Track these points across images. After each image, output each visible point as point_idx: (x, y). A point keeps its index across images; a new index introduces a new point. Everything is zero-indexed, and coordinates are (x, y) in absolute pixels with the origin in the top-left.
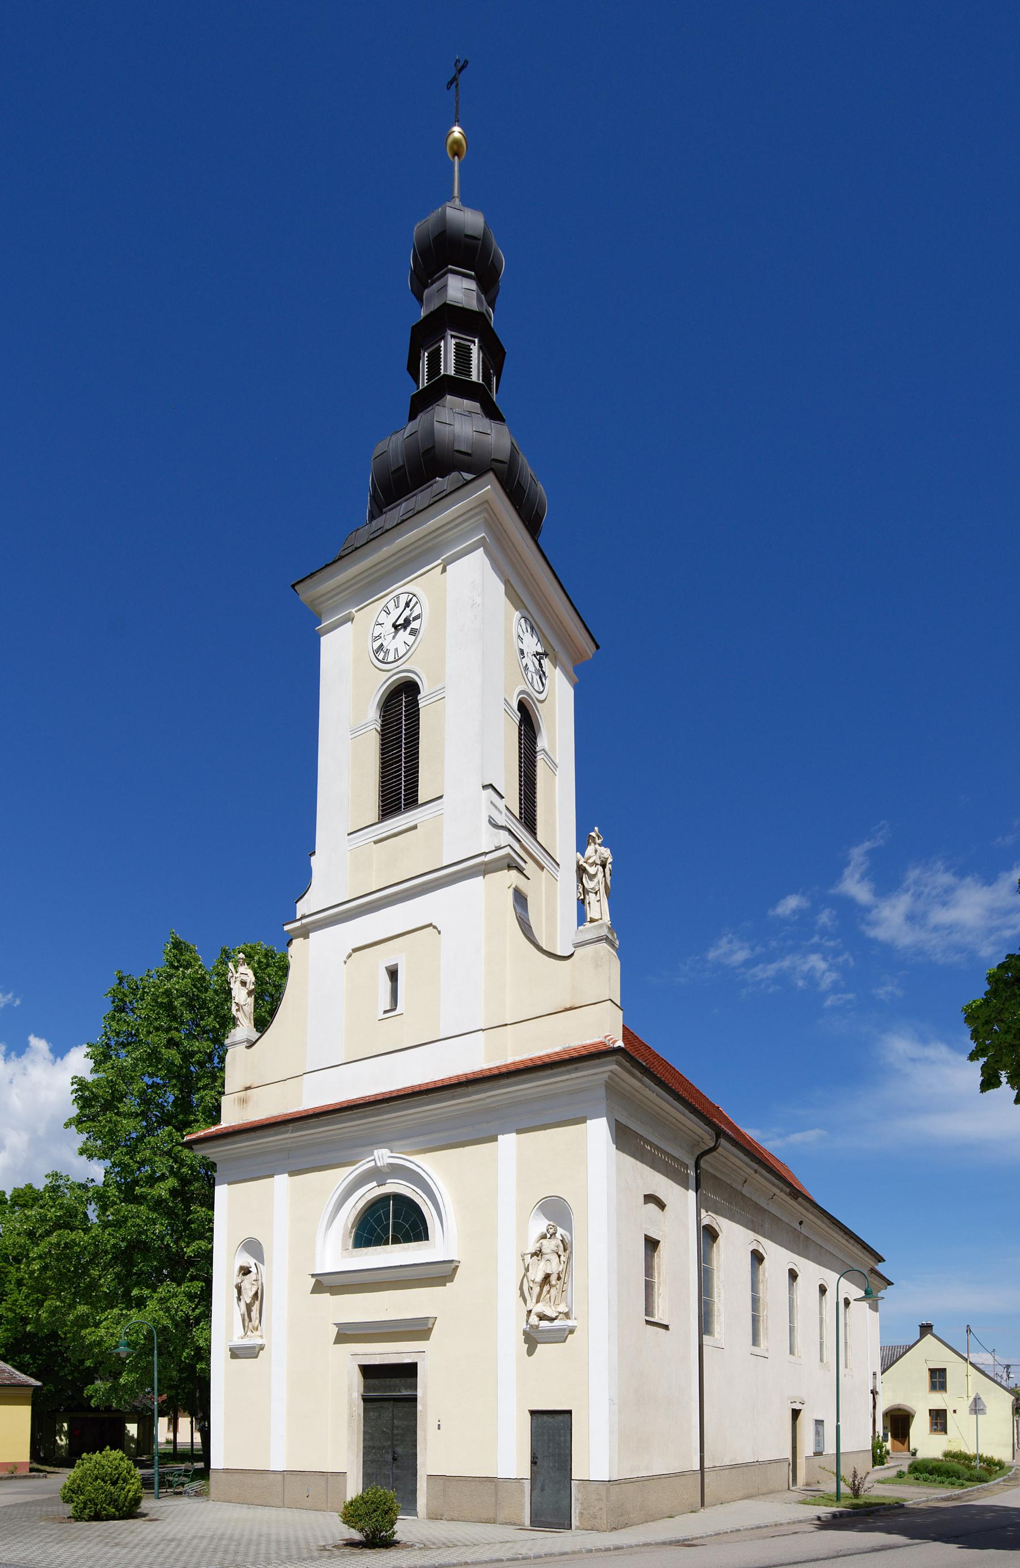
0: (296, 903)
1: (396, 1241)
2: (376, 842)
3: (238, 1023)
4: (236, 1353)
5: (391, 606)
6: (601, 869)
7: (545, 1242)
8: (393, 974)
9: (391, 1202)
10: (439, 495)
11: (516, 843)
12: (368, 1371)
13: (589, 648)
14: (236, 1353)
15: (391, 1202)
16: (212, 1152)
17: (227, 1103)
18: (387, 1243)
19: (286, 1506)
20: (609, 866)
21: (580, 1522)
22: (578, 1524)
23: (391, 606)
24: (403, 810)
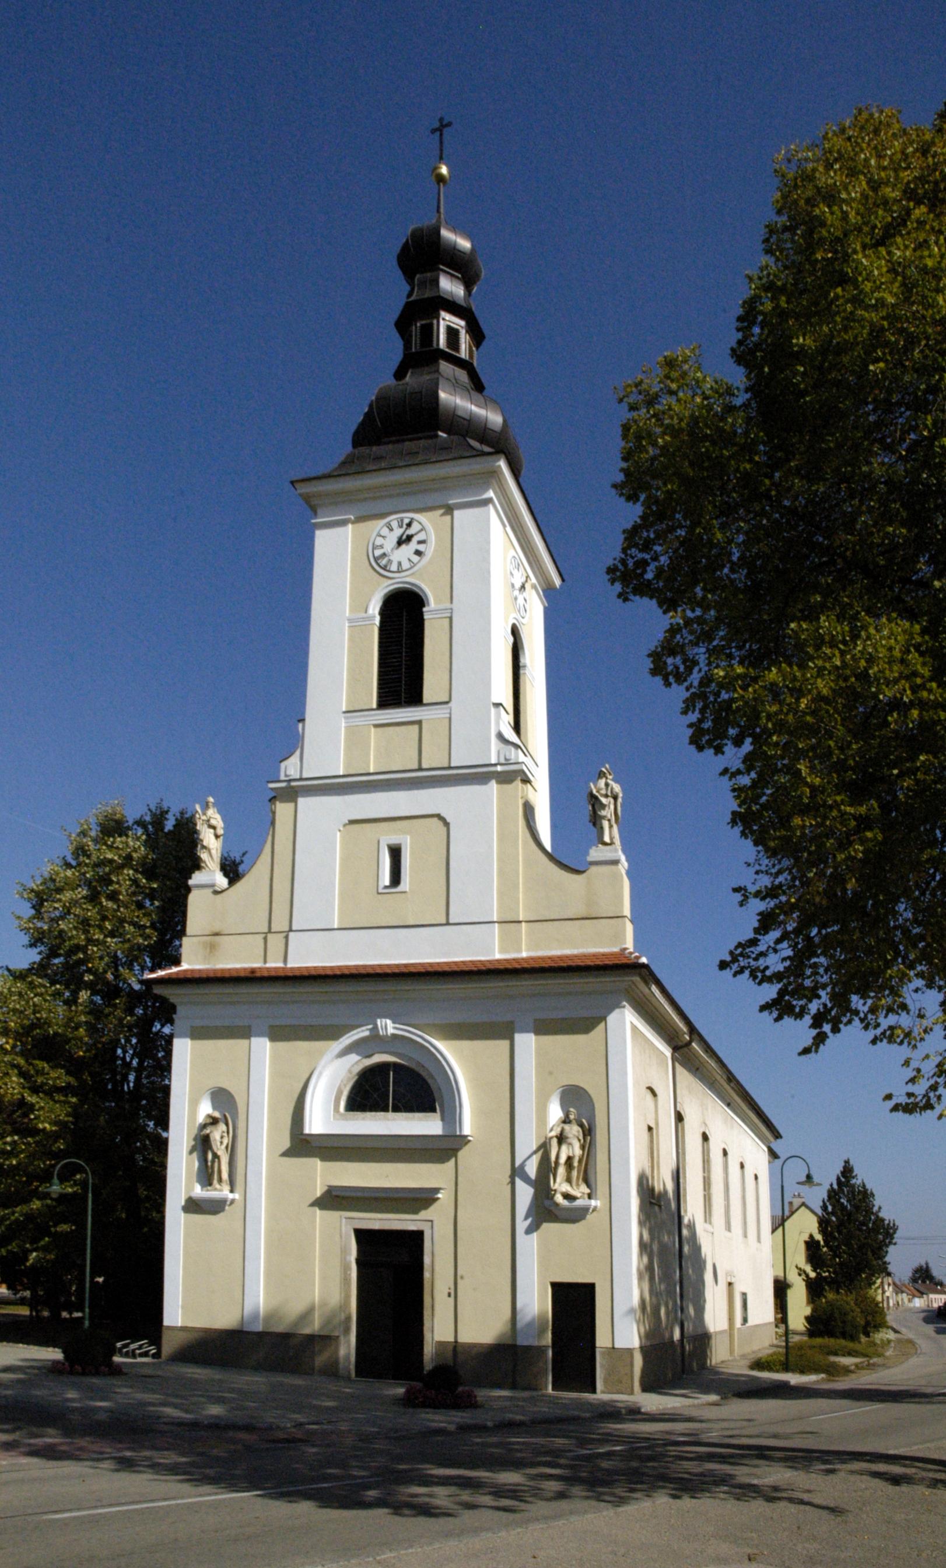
0: (281, 762)
1: (396, 1109)
2: (376, 726)
3: (203, 865)
4: (193, 1206)
5: (395, 524)
6: (612, 801)
7: (567, 1127)
8: (396, 853)
9: (391, 1073)
10: (754, 1203)
11: (567, 952)
12: (363, 1236)
13: (557, 582)
14: (193, 1206)
15: (391, 1073)
16: (170, 993)
17: (188, 947)
18: (385, 1109)
19: (448, 605)
20: (620, 800)
21: (606, 1387)
22: (603, 1388)
23: (395, 524)
24: (236, 1196)
